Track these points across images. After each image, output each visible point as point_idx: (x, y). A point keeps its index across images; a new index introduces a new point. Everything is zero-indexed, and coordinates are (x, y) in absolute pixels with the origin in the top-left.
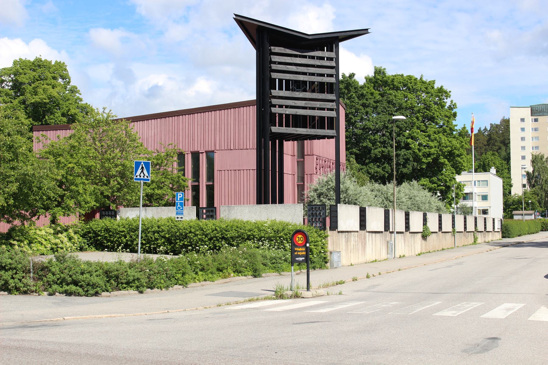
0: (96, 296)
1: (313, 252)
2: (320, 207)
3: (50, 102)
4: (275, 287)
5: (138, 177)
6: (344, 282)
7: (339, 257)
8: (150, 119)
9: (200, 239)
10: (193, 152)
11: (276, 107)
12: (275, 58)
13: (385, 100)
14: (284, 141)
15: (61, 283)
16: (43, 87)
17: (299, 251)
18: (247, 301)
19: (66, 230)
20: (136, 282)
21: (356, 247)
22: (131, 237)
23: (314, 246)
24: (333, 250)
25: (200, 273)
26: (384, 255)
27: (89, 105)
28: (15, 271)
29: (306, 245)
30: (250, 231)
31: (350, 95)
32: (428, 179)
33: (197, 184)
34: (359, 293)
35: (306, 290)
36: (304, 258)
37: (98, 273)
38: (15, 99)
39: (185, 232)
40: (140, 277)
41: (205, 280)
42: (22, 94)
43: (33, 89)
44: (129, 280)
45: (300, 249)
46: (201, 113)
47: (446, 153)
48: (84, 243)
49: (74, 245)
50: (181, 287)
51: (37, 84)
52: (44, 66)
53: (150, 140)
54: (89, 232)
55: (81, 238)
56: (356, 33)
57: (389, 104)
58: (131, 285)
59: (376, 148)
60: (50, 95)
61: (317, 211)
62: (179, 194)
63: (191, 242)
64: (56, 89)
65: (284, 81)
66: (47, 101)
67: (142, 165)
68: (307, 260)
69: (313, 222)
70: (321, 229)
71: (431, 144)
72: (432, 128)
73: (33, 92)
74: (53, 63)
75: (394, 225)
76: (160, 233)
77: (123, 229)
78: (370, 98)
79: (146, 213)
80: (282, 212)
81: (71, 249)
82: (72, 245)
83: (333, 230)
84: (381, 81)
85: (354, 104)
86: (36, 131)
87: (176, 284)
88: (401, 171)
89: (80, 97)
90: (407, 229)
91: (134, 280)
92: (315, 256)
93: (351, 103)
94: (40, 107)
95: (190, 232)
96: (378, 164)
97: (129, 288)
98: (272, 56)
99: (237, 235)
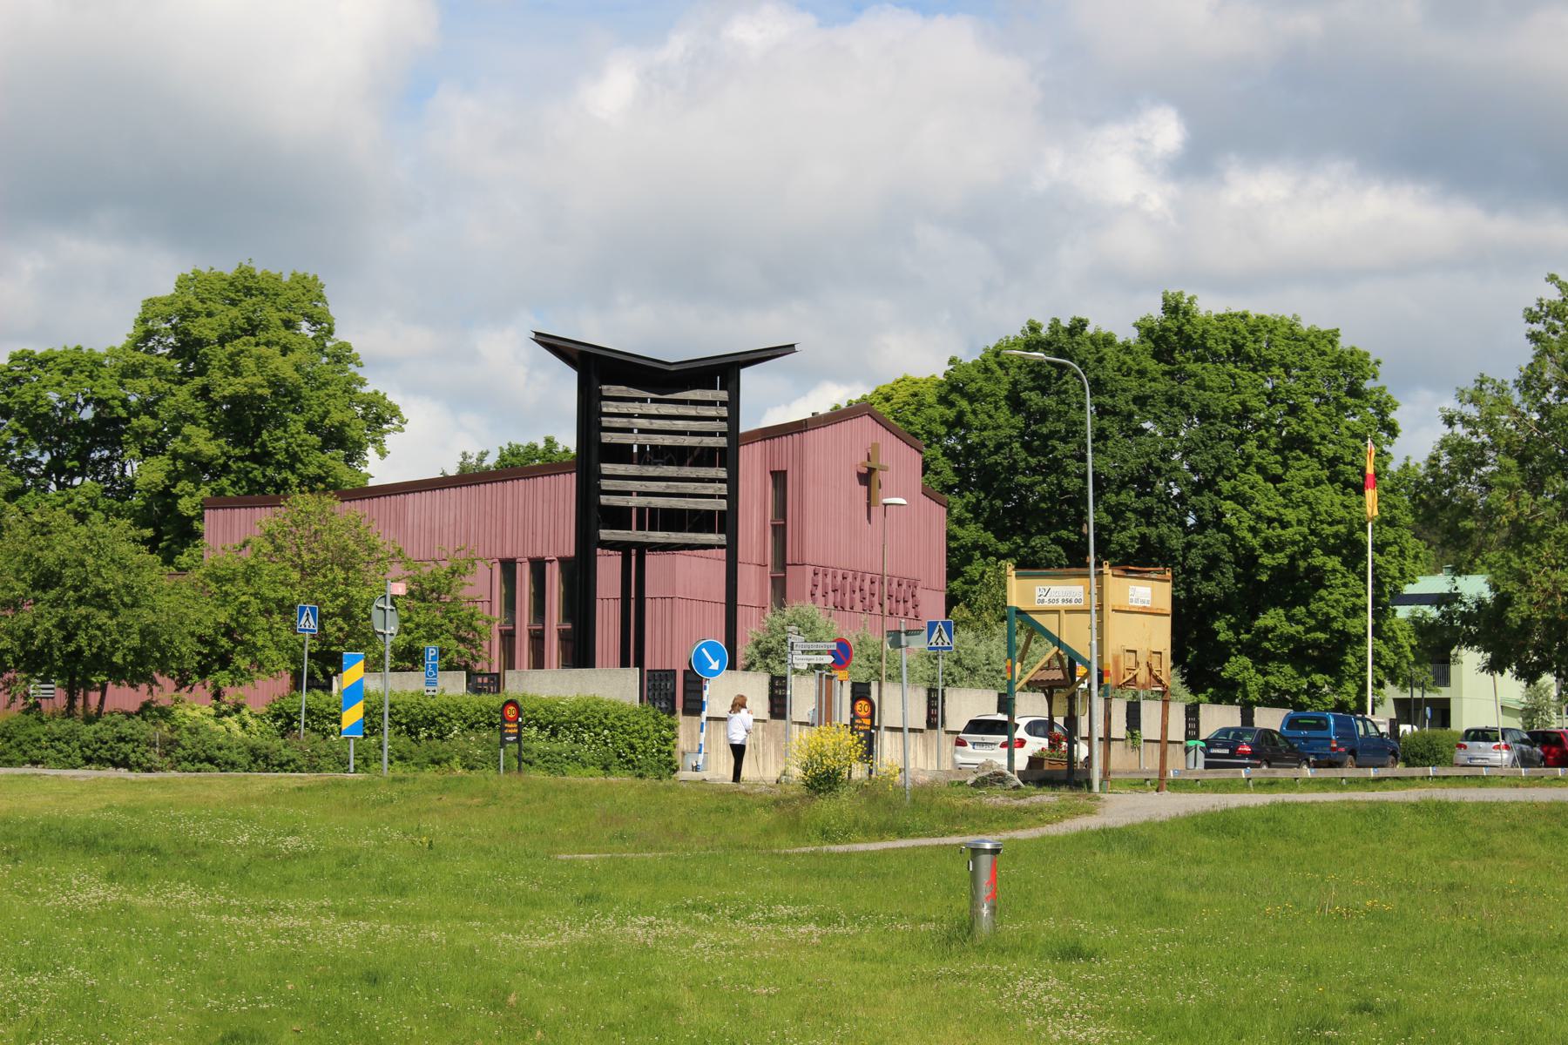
15: (193, 760)
19: (237, 711)
25: (396, 762)
28: (136, 744)
32: (1281, 611)
37: (240, 750)
38: (181, 383)
42: (202, 371)
45: (511, 726)
46: (550, 475)
47: (1332, 541)
53: (445, 531)
56: (769, 354)
59: (1124, 529)
60: (275, 376)
64: (292, 357)
66: (266, 392)
71: (1290, 515)
72: (1304, 469)
73: (229, 367)
74: (286, 278)
86: (209, 508)
88: (1198, 590)
89: (360, 375)
95: (441, 715)
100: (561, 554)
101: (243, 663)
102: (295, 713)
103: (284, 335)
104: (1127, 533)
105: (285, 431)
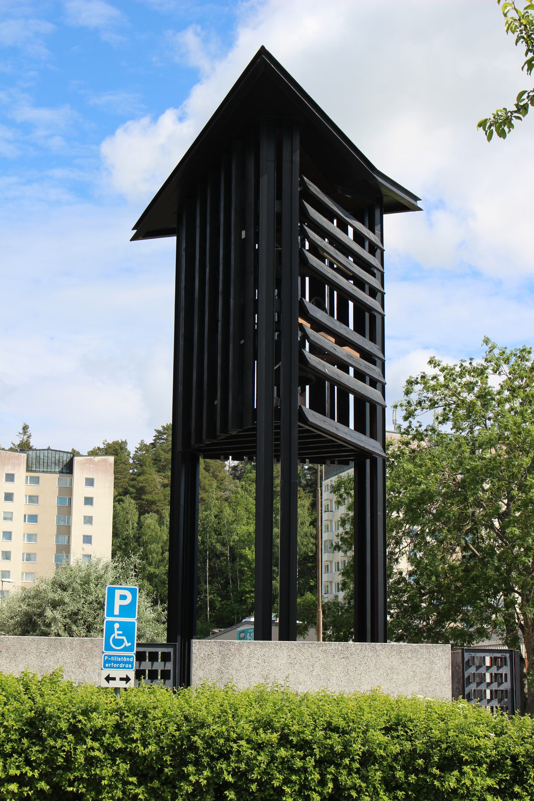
62: (118, 593)
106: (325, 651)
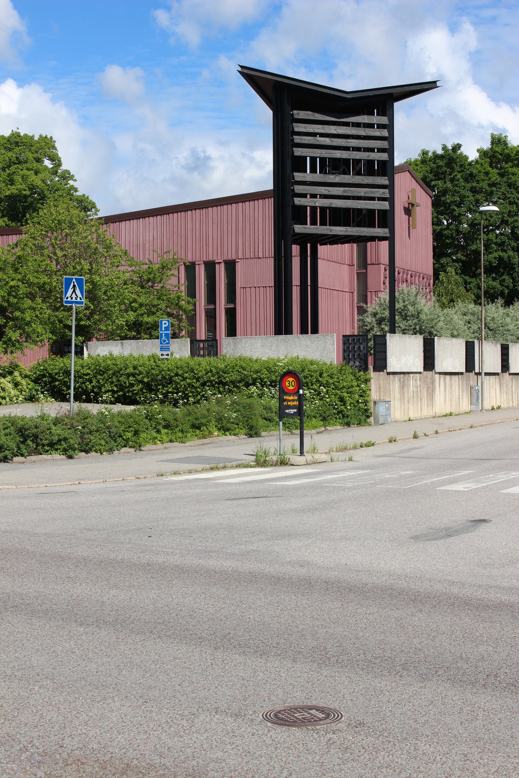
0: (5, 462)
1: (345, 402)
2: (359, 339)
3: (31, 194)
4: (256, 450)
5: (69, 299)
6: (373, 445)
7: (388, 409)
8: (147, 217)
9: (189, 384)
10: (207, 262)
11: (307, 197)
12: (299, 128)
13: (505, 183)
14: (318, 245)
16: (21, 173)
17: (290, 401)
18: (206, 470)
19: (11, 373)
20: (63, 443)
21: (417, 395)
22: (98, 382)
23: (348, 393)
24: (380, 399)
25: (164, 431)
26: (465, 405)
27: (88, 198)
29: (298, 392)
30: (257, 372)
31: (452, 176)
33: (233, 306)
34: (380, 459)
35: (300, 454)
36: (295, 410)
37: (7, 431)
39: (169, 375)
40: (67, 436)
41: (171, 441)
43: (8, 177)
44: (53, 440)
45: (291, 398)
48: (37, 390)
49: (21, 394)
50: (132, 450)
51: (13, 168)
52: (24, 144)
53: (147, 246)
54: (44, 376)
55: (32, 384)
56: (418, 88)
57: (510, 188)
58: (56, 447)
60: (32, 185)
61: (355, 344)
62: (163, 322)
63: (178, 389)
64: (40, 175)
65: (318, 159)
66: (28, 193)
67: (74, 282)
68: (300, 413)
69: (350, 359)
70: (361, 368)
73: (8, 180)
74: (36, 138)
75: (482, 363)
76: (136, 376)
77: (88, 371)
78: (483, 180)
79: (123, 348)
80: (307, 346)
81: (17, 399)
82: (19, 393)
83: (379, 371)
84: (501, 154)
85: (457, 189)
87: (125, 446)
90: (504, 369)
91: (60, 441)
92: (349, 407)
93: (454, 187)
94: (19, 201)
95: (177, 375)
96: (494, 275)
97: (53, 452)
98: (294, 124)
99: (239, 378)
100: (226, 258)
101: (14, 335)
102: (56, 374)
103: (35, 165)
104: (493, 255)
105: (38, 214)
106: (277, 340)
